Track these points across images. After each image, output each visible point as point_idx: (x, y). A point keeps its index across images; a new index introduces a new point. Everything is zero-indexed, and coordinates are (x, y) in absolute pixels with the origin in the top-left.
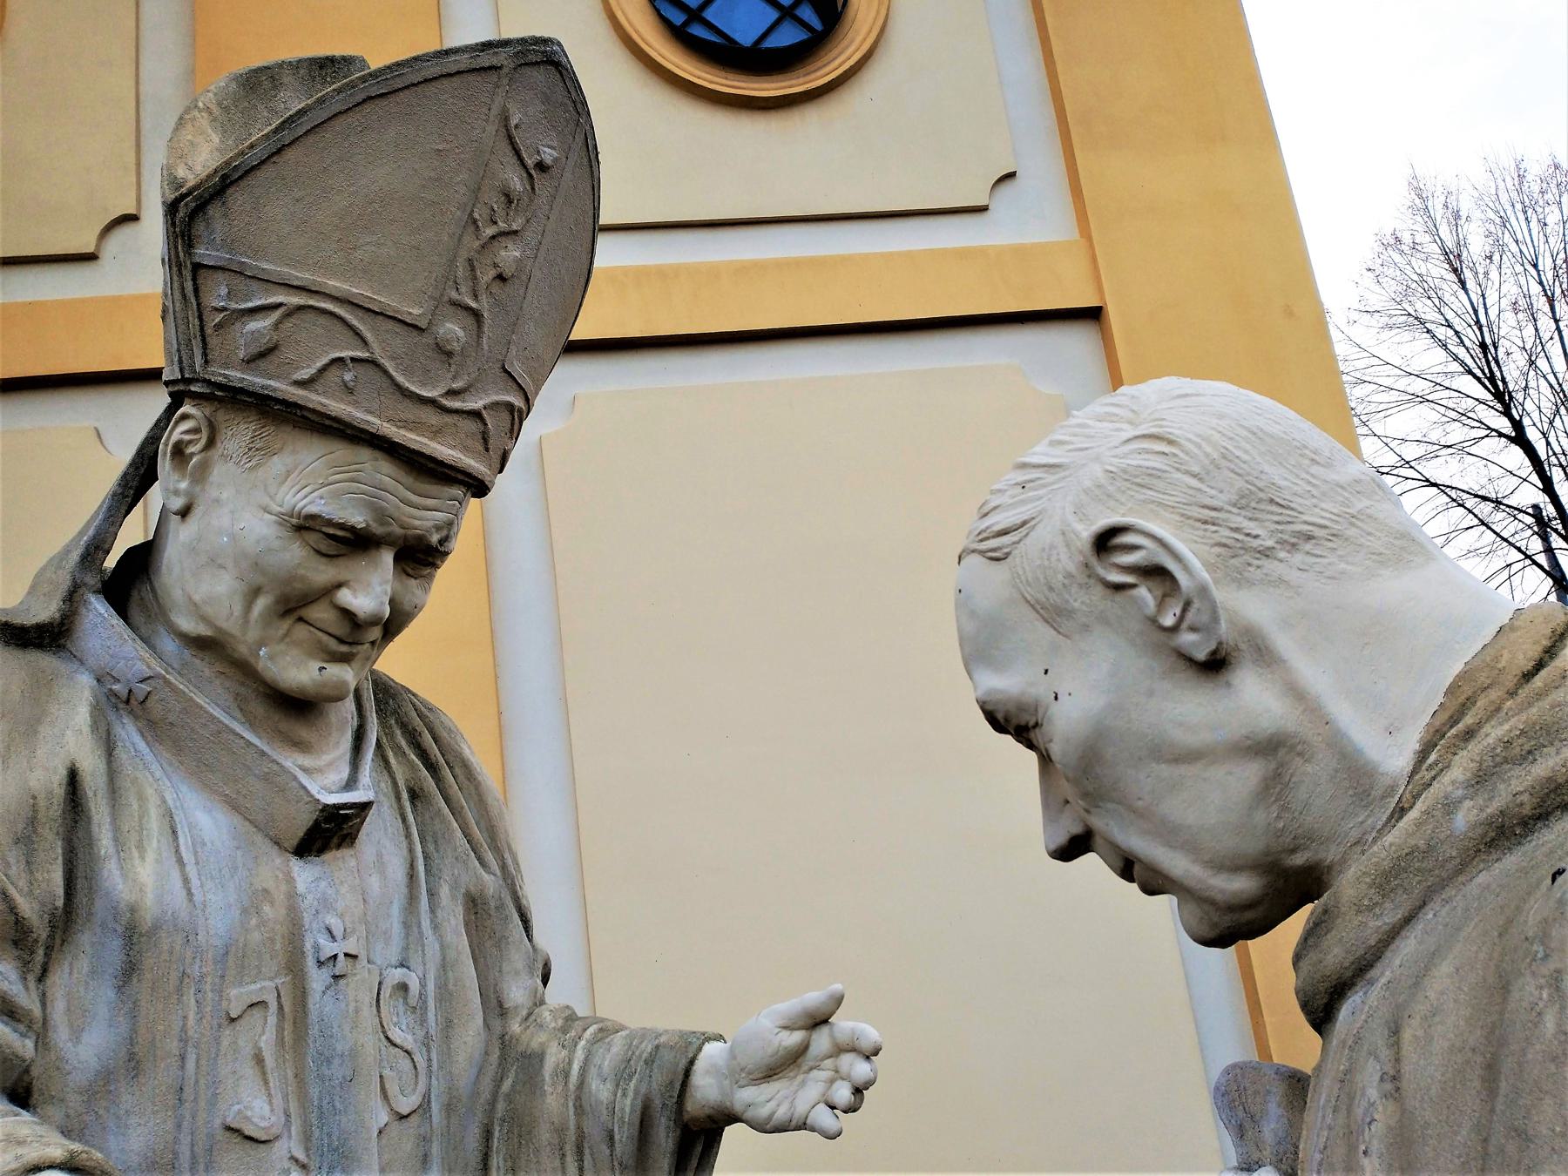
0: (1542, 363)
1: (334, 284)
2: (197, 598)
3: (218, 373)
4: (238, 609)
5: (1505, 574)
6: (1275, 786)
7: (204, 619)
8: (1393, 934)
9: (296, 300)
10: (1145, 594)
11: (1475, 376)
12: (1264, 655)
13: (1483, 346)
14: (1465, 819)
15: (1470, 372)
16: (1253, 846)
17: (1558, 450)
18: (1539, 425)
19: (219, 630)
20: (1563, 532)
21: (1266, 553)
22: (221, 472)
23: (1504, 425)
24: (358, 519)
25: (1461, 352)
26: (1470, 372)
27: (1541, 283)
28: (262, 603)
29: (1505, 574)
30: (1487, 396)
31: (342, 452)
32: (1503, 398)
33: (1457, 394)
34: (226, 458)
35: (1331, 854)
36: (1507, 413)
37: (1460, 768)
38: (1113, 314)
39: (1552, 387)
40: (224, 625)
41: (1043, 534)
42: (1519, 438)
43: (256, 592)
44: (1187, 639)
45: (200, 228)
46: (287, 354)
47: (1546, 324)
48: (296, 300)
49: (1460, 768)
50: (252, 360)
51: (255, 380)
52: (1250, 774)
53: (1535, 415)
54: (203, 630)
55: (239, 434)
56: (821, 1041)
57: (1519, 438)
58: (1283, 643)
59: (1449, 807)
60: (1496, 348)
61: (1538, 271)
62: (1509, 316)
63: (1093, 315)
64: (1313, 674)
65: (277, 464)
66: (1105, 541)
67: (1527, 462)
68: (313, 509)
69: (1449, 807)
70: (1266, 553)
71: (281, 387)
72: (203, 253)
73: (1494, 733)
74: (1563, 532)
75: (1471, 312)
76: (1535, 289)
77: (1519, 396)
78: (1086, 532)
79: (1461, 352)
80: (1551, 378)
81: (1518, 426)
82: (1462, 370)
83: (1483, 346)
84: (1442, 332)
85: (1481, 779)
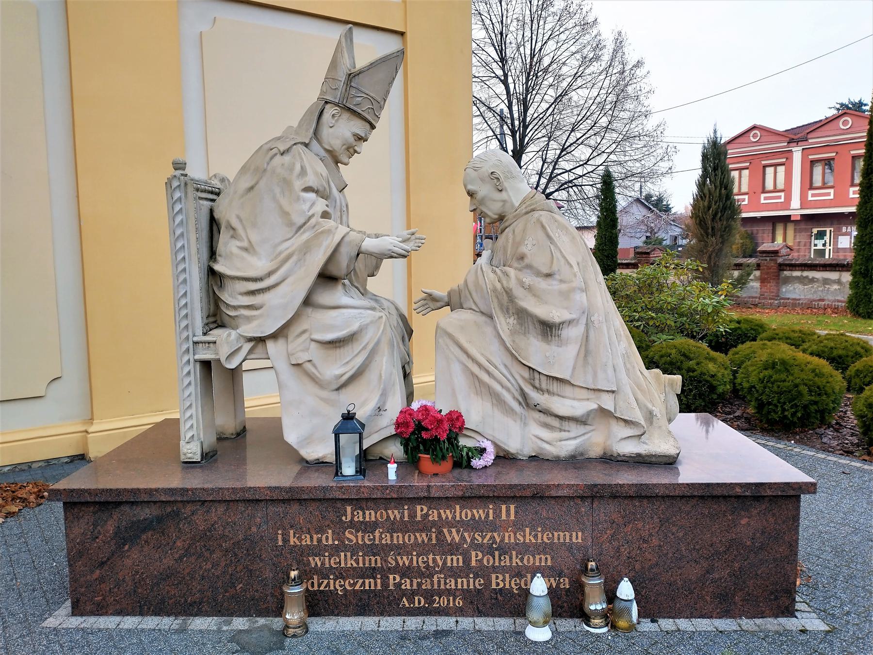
0: (522, 49)
1: (372, 94)
2: (331, 143)
3: (348, 105)
4: (340, 147)
5: (486, 140)
6: (503, 205)
7: (331, 147)
8: (514, 222)
9: (366, 96)
10: (495, 180)
11: (495, 48)
12: (506, 190)
13: (501, 34)
14: (524, 211)
15: (493, 45)
16: (499, 212)
17: (518, 91)
18: (513, 77)
19: (334, 149)
20: (510, 127)
21: (509, 178)
22: (341, 121)
23: (500, 73)
24: (363, 135)
25: (493, 35)
26: (493, 45)
27: (530, 11)
28: (344, 147)
29: (486, 140)
30: (497, 58)
31: (364, 123)
32: (503, 60)
33: (485, 53)
34: (342, 119)
35: (507, 214)
36: (503, 69)
37: (524, 206)
38: (409, 35)
39: (522, 60)
40: (336, 149)
41: (483, 169)
42: (505, 83)
43: (343, 145)
44: (499, 187)
45: (353, 80)
46: (362, 105)
47: (528, 34)
48: (366, 96)
49: (524, 206)
50: (355, 105)
51: (355, 108)
52: (501, 204)
53: (513, 71)
54: (330, 149)
55: (346, 115)
56: (413, 237)
57: (505, 83)
58: (509, 190)
59: (523, 210)
60: (506, 36)
61: (531, 5)
62: (515, 23)
63: (402, 34)
64: (511, 194)
65: (352, 123)
66: (492, 173)
67: (505, 92)
68: (358, 133)
69: (523, 210)
70: (509, 178)
71: (359, 111)
72: (353, 84)
73: (528, 203)
74: (510, 127)
75: (501, 15)
76: (528, 12)
77: (510, 62)
78: (490, 172)
79: (493, 35)
80: (523, 55)
81: (506, 75)
82: (490, 42)
83: (501, 34)
84: (488, 22)
85: (526, 208)
